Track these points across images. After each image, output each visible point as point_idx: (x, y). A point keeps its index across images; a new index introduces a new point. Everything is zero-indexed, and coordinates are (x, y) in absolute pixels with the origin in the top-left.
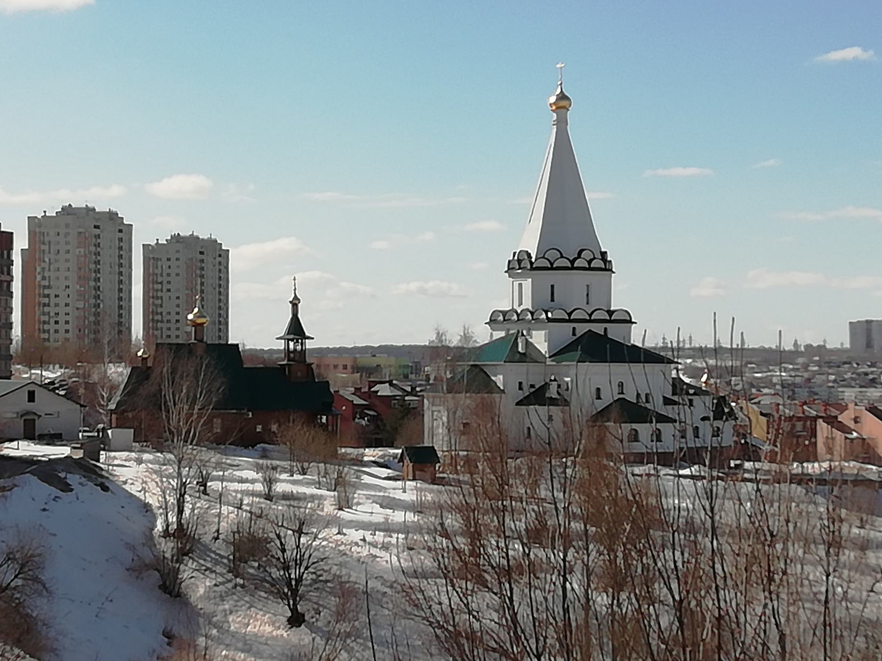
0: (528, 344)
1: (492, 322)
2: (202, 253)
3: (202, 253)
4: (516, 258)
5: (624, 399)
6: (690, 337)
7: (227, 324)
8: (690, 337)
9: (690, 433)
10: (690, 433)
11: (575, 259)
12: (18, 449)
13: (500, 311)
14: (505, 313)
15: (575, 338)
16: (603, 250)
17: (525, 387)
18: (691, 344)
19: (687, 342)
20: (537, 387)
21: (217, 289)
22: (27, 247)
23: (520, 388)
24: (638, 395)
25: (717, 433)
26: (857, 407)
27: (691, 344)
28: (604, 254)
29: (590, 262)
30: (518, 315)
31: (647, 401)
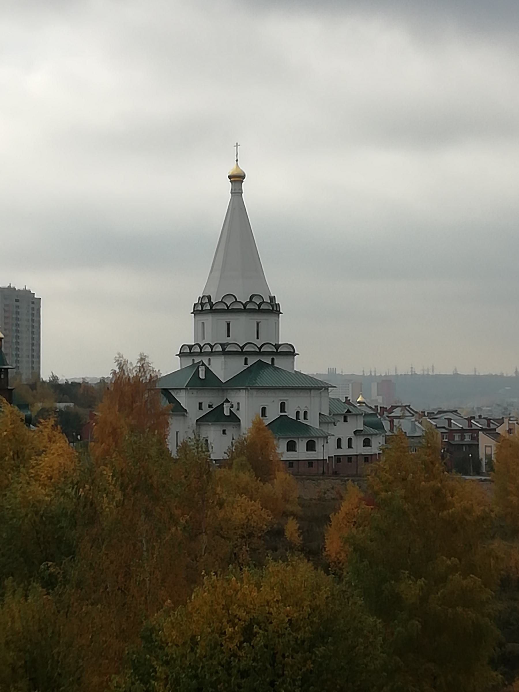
0: (208, 371)
1: (181, 354)
2: (17, 301)
3: (17, 301)
4: (200, 302)
5: (286, 416)
6: (433, 366)
7: (39, 357)
8: (433, 366)
9: (344, 444)
10: (344, 444)
11: (247, 303)
12: (486, 446)
13: (187, 345)
14: (190, 347)
15: (247, 366)
16: (272, 295)
17: (205, 406)
18: (433, 371)
19: (431, 370)
20: (214, 407)
21: (30, 329)
22: (36, 297)
23: (200, 408)
24: (298, 413)
25: (367, 443)
26: (510, 422)
27: (433, 371)
28: (273, 299)
29: (259, 306)
30: (201, 348)
31: (305, 418)
